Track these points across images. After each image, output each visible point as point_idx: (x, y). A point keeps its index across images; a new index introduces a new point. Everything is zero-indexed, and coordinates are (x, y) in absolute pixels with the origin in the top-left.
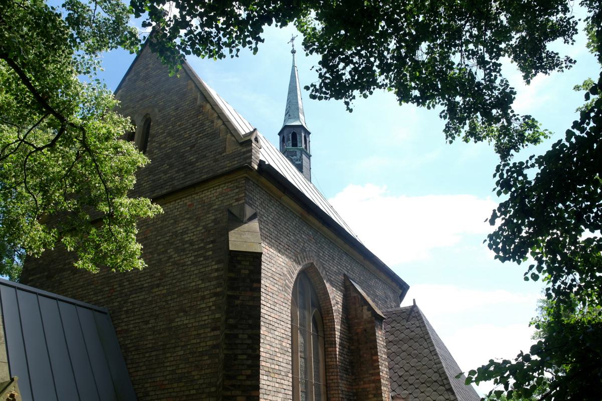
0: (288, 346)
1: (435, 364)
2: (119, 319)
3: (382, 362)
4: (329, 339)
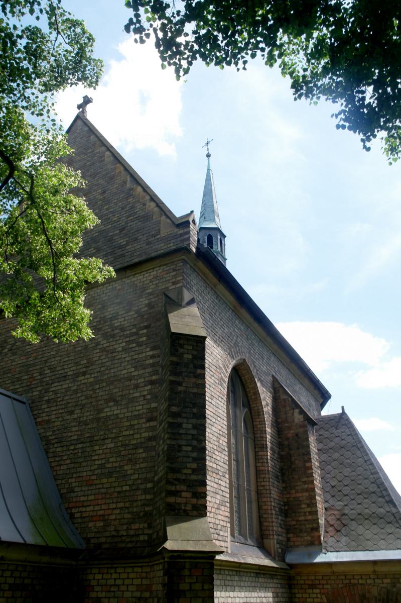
0: (225, 444)
1: (372, 474)
2: (40, 410)
3: (315, 469)
4: (259, 443)
